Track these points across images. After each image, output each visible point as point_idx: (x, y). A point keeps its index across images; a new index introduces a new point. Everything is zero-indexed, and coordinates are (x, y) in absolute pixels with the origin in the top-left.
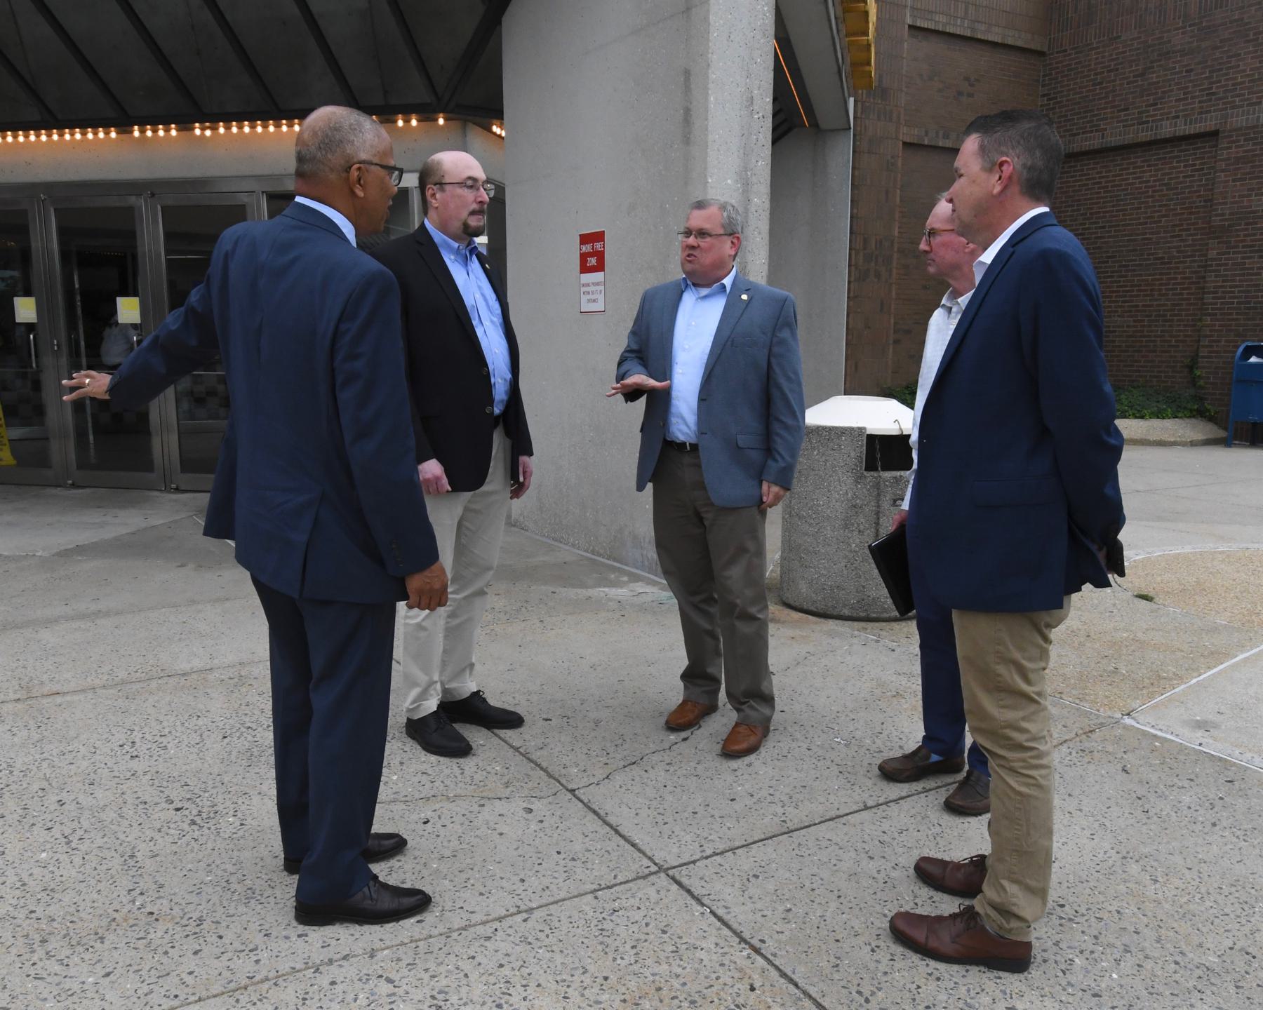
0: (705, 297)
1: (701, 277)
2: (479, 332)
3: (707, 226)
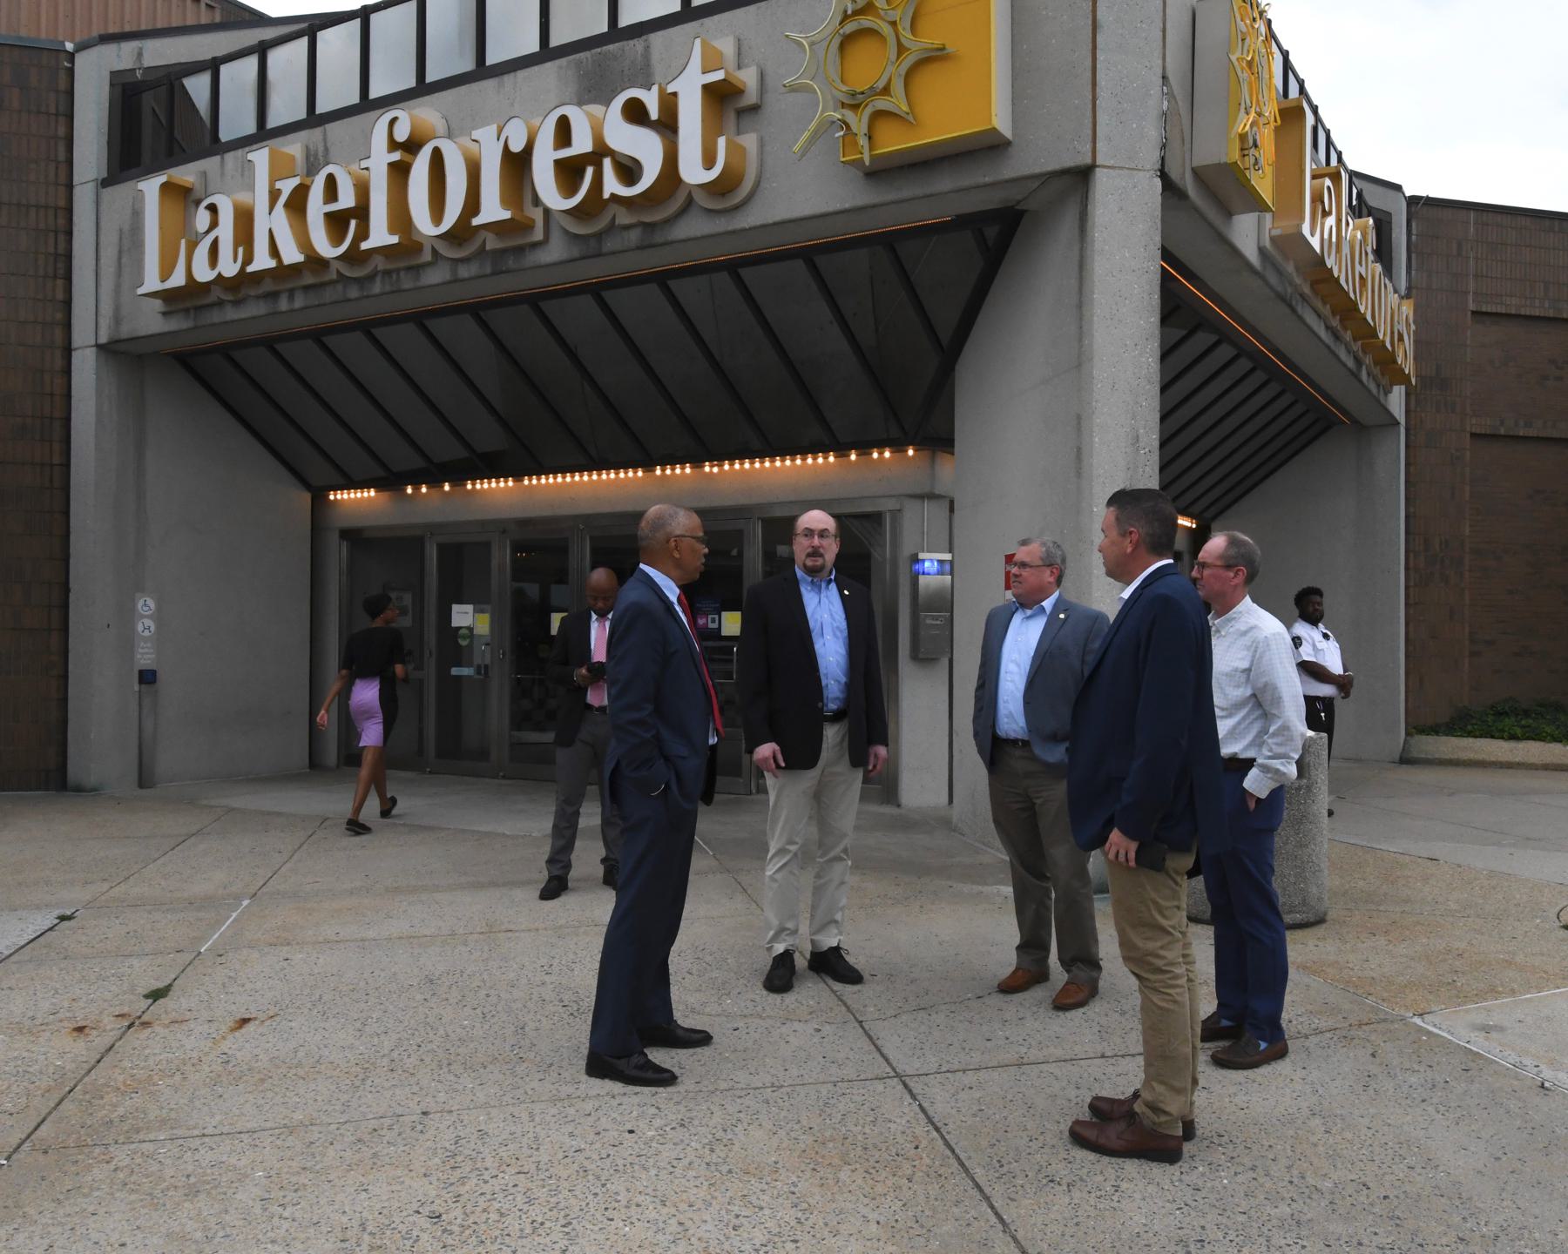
0: (1029, 618)
1: (1028, 602)
2: (818, 647)
3: (1027, 560)
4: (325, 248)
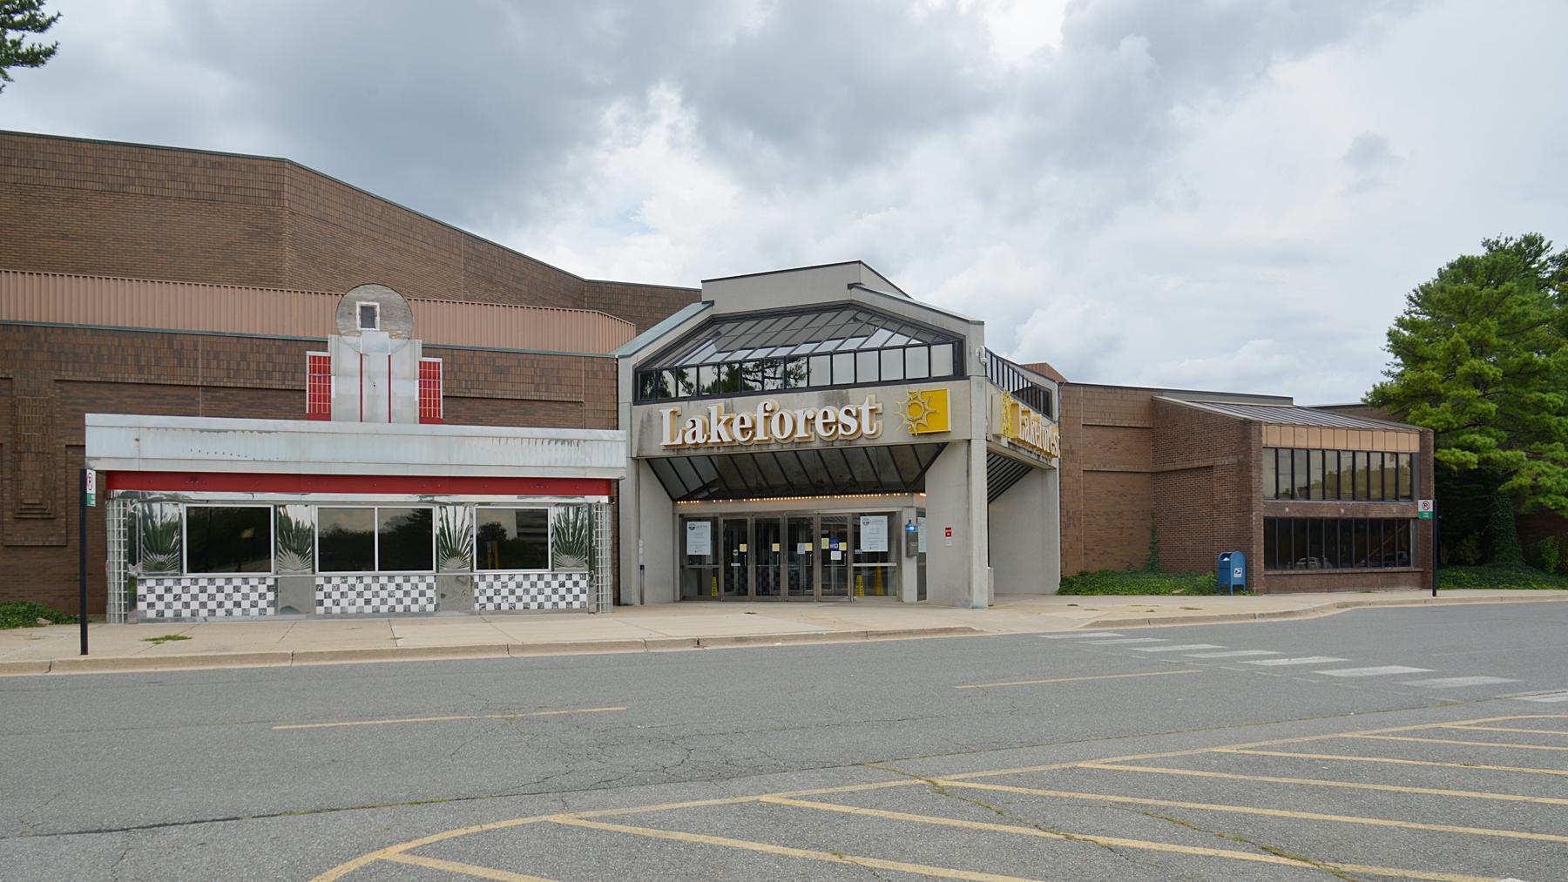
4: (739, 438)
